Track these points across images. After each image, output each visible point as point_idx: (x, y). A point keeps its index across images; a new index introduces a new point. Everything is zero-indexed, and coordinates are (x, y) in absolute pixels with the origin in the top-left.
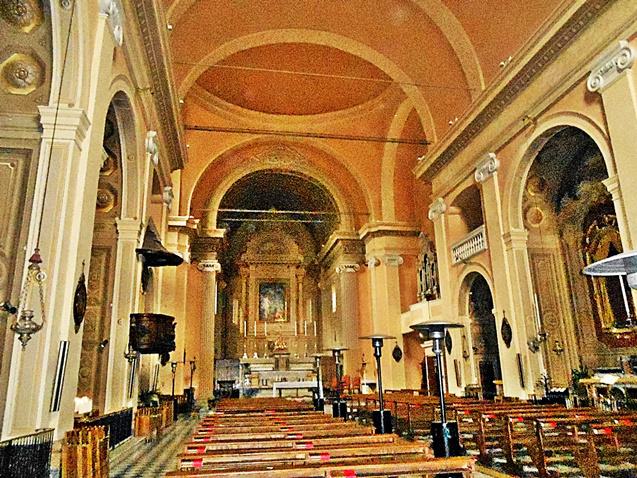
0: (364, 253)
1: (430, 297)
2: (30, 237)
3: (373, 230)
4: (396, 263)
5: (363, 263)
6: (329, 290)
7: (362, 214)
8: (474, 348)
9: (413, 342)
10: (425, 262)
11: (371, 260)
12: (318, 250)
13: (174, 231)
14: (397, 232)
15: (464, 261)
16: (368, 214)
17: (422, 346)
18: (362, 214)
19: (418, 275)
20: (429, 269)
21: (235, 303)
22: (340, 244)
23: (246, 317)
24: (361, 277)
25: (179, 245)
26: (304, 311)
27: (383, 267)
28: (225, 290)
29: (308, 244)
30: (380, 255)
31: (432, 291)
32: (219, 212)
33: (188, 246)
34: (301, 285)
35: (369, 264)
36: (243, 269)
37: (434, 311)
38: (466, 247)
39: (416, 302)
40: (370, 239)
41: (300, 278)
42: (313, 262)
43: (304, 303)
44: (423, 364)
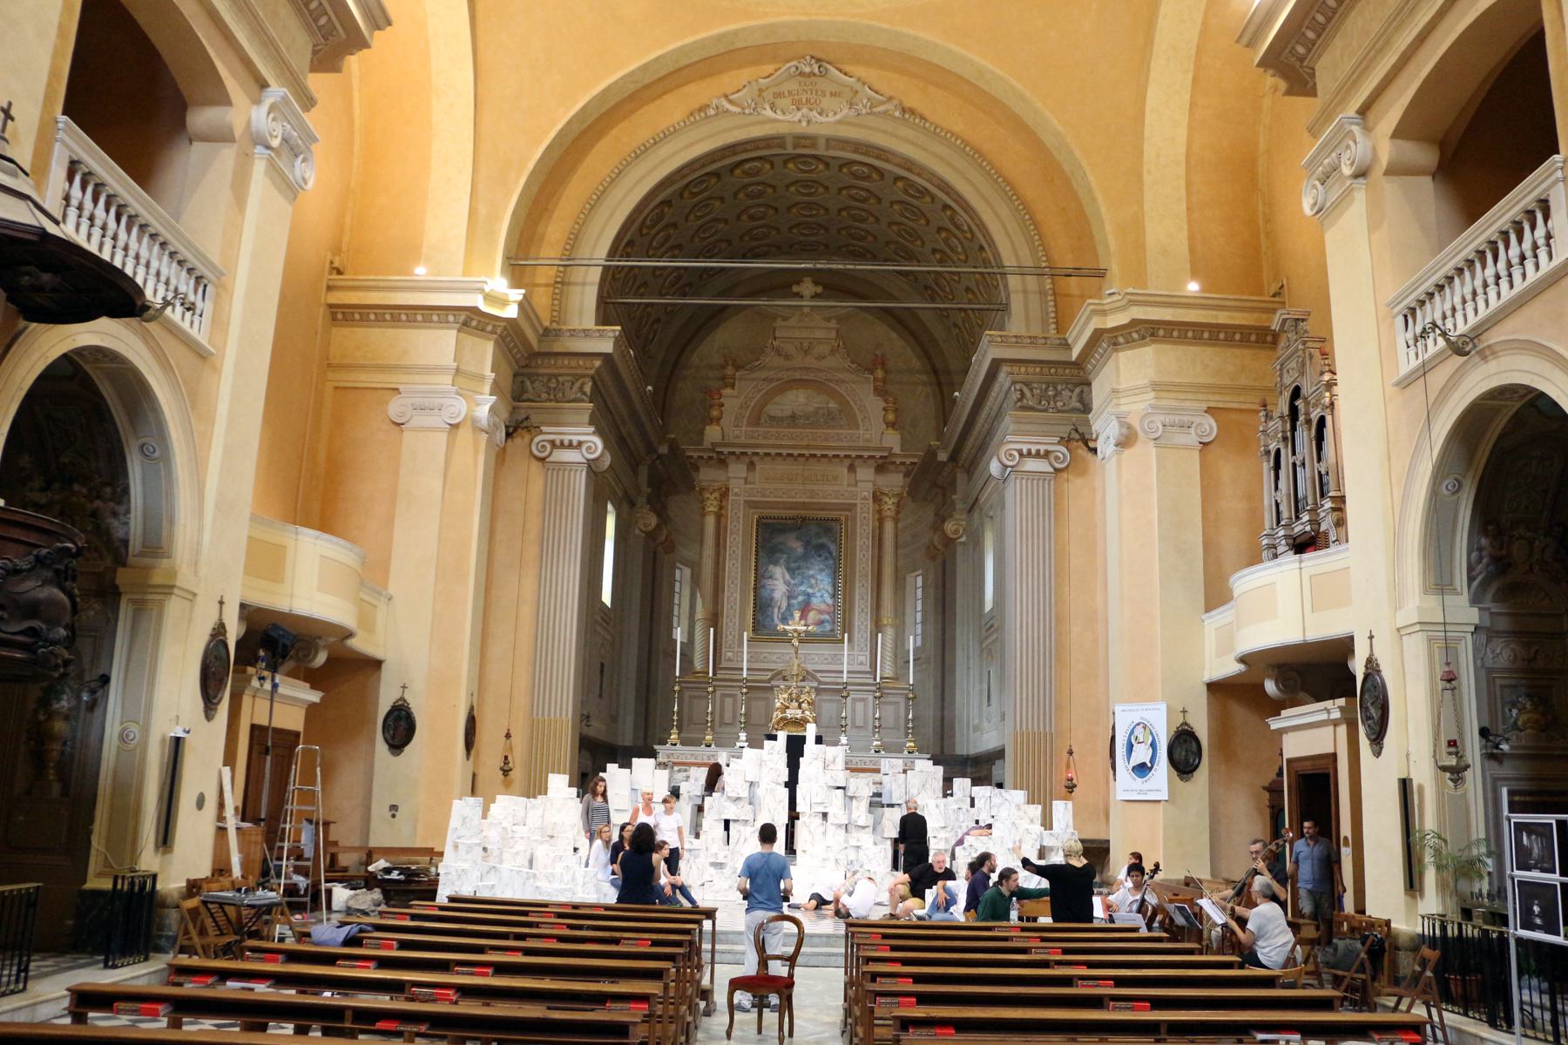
0: (1086, 408)
1: (1303, 545)
2: (1473, 815)
3: (1112, 321)
4: (1192, 438)
5: (1087, 442)
6: (977, 545)
7: (1077, 272)
8: (1484, 732)
9: (1240, 714)
10: (1294, 412)
11: (1105, 428)
12: (945, 407)
13: (444, 323)
14: (1183, 326)
15: (1458, 348)
16: (1100, 274)
17: (1275, 724)
18: (1077, 272)
19: (1267, 466)
20: (1304, 436)
21: (683, 575)
22: (1003, 377)
23: (715, 619)
24: (1074, 486)
25: (458, 370)
26: (899, 613)
27: (1145, 451)
28: (651, 536)
29: (920, 400)
30: (1136, 407)
31: (1315, 522)
32: (606, 269)
33: (490, 375)
34: (889, 527)
35: (1099, 445)
36: (707, 476)
37: (1320, 596)
38: (1462, 288)
39: (1254, 559)
40: (1105, 359)
41: (889, 504)
42: (931, 454)
43: (899, 582)
44: (1274, 790)
